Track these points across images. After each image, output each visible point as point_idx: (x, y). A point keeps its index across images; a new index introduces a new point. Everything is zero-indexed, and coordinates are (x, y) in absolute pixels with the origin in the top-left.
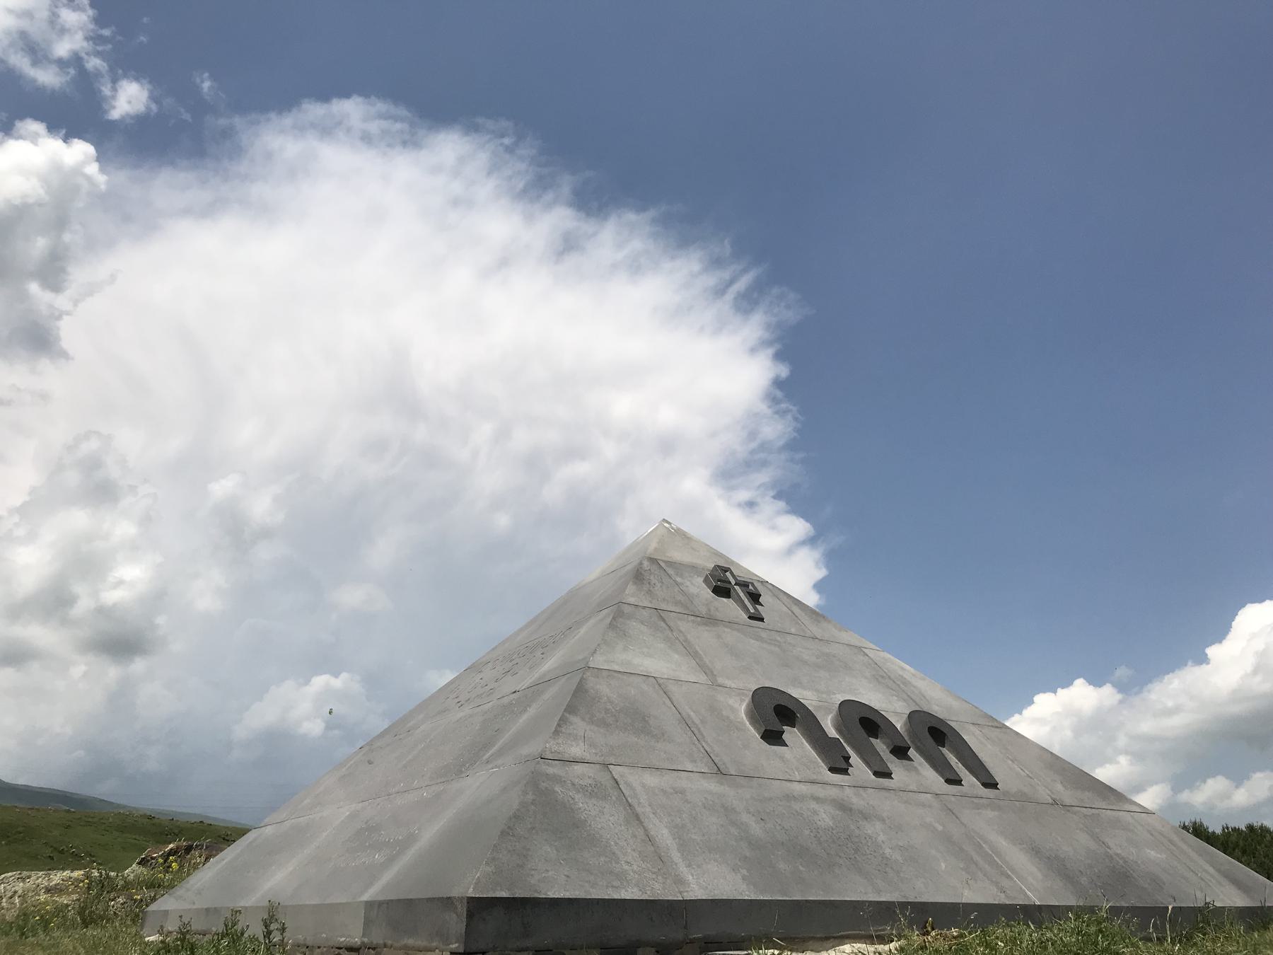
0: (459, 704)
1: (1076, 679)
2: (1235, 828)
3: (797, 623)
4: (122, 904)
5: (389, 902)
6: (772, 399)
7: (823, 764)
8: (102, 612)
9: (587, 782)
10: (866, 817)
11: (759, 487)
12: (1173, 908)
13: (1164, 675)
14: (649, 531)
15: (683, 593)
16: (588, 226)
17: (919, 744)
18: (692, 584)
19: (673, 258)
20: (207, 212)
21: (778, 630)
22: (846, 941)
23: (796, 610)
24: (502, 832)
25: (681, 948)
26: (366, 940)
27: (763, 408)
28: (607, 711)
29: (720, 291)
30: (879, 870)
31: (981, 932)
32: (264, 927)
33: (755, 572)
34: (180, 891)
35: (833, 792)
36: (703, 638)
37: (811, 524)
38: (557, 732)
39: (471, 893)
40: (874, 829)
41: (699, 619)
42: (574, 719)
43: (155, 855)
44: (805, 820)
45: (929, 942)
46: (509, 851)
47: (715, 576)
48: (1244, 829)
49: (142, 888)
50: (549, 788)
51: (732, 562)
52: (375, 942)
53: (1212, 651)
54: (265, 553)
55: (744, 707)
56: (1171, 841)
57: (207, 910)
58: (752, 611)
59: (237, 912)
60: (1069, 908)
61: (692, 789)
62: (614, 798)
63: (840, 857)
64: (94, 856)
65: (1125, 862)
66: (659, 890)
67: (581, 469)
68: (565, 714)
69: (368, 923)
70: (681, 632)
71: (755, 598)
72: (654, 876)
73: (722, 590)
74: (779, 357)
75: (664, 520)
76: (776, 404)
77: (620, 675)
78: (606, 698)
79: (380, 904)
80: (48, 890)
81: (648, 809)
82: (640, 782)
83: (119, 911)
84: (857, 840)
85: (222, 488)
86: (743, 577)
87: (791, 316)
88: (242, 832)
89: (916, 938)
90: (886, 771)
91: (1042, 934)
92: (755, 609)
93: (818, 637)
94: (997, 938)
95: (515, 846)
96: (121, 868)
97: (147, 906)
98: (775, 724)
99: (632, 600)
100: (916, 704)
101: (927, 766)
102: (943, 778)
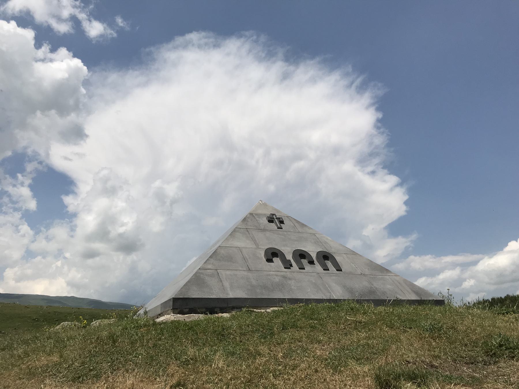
8: (121, 235)
11: (376, 165)
16: (292, 68)
20: (145, 84)
23: (296, 224)
27: (374, 132)
29: (350, 86)
40: (292, 283)
41: (260, 230)
42: (211, 259)
54: (179, 211)
67: (301, 164)
73: (271, 220)
74: (378, 109)
87: (380, 93)
90: (303, 267)
92: (280, 225)
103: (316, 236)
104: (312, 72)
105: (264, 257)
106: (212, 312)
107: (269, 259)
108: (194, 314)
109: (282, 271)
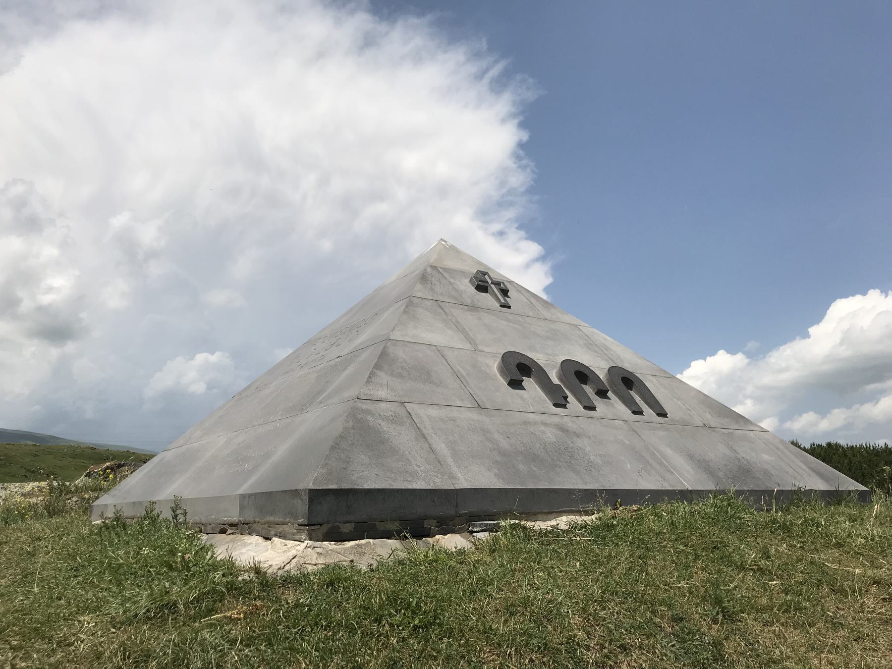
0: (300, 366)
1: (719, 350)
2: (819, 445)
3: (533, 309)
4: (75, 502)
5: (256, 495)
6: (517, 157)
7: (549, 401)
8: (41, 309)
9: (389, 413)
10: (578, 436)
11: (507, 221)
12: (777, 490)
13: (780, 346)
14: (431, 248)
15: (456, 290)
16: (383, 27)
17: (615, 388)
18: (461, 283)
19: (445, 52)
21: (521, 314)
22: (563, 514)
23: (533, 300)
24: (332, 447)
25: (453, 520)
26: (241, 519)
27: (510, 163)
28: (402, 368)
29: (479, 76)
30: (586, 469)
31: (652, 507)
32: (172, 512)
33: (505, 276)
34: (113, 492)
35: (556, 420)
36: (469, 320)
37: (542, 247)
38: (368, 382)
39: (311, 486)
40: (582, 443)
41: (466, 307)
42: (381, 374)
43: (96, 470)
44: (537, 437)
45: (618, 514)
46: (337, 459)
47: (477, 278)
48: (825, 445)
49: (88, 492)
50: (364, 418)
51: (489, 269)
52: (247, 520)
53: (812, 330)
54: (156, 270)
55: (496, 365)
56: (777, 448)
57: (134, 503)
58: (503, 301)
59: (153, 503)
60: (710, 491)
61: (461, 418)
62: (407, 424)
63: (560, 461)
64: (56, 474)
65: (748, 462)
66: (439, 483)
67: (382, 208)
68: (374, 370)
69: (242, 508)
70: (453, 315)
71: (505, 292)
72: (435, 474)
73: (482, 287)
74: (522, 125)
75: (441, 239)
76: (520, 160)
77: (411, 344)
78: (402, 359)
79: (250, 495)
80: (23, 495)
81: (431, 431)
82: (424, 414)
83: (74, 507)
84: (571, 450)
85: (120, 221)
86: (497, 278)
87: (531, 96)
88: (152, 456)
89: (609, 512)
91: (692, 507)
92: (505, 300)
93: (548, 318)
94: (663, 510)
95: (340, 456)
96: (72, 479)
97: (93, 502)
98: (517, 376)
99: (419, 294)
100: (614, 362)
101: (620, 403)
102: (631, 411)
103: (580, 330)
104: (418, 41)
105: (501, 375)
106: (420, 533)
107: (516, 380)
108: (371, 541)
109: (547, 411)
